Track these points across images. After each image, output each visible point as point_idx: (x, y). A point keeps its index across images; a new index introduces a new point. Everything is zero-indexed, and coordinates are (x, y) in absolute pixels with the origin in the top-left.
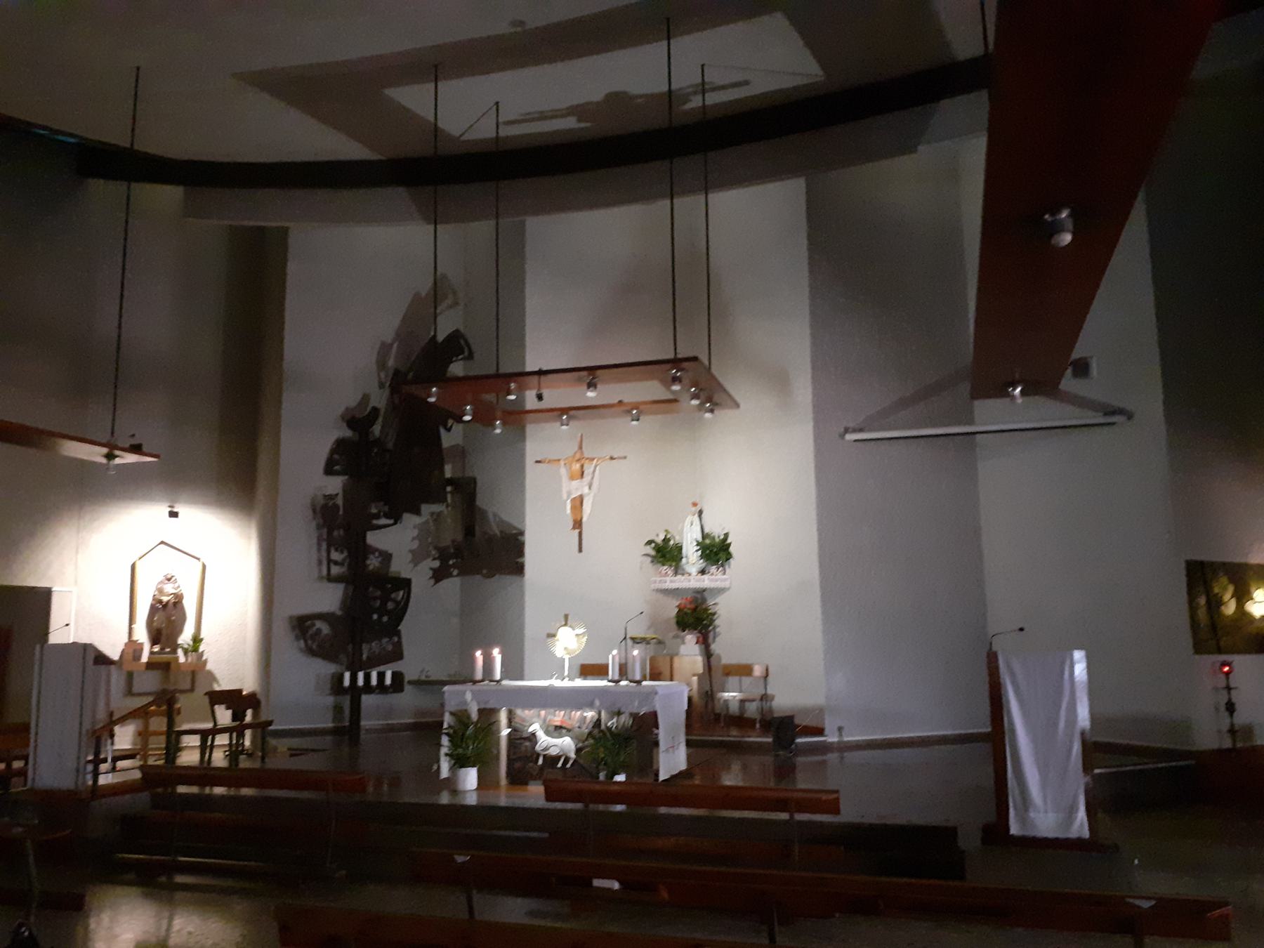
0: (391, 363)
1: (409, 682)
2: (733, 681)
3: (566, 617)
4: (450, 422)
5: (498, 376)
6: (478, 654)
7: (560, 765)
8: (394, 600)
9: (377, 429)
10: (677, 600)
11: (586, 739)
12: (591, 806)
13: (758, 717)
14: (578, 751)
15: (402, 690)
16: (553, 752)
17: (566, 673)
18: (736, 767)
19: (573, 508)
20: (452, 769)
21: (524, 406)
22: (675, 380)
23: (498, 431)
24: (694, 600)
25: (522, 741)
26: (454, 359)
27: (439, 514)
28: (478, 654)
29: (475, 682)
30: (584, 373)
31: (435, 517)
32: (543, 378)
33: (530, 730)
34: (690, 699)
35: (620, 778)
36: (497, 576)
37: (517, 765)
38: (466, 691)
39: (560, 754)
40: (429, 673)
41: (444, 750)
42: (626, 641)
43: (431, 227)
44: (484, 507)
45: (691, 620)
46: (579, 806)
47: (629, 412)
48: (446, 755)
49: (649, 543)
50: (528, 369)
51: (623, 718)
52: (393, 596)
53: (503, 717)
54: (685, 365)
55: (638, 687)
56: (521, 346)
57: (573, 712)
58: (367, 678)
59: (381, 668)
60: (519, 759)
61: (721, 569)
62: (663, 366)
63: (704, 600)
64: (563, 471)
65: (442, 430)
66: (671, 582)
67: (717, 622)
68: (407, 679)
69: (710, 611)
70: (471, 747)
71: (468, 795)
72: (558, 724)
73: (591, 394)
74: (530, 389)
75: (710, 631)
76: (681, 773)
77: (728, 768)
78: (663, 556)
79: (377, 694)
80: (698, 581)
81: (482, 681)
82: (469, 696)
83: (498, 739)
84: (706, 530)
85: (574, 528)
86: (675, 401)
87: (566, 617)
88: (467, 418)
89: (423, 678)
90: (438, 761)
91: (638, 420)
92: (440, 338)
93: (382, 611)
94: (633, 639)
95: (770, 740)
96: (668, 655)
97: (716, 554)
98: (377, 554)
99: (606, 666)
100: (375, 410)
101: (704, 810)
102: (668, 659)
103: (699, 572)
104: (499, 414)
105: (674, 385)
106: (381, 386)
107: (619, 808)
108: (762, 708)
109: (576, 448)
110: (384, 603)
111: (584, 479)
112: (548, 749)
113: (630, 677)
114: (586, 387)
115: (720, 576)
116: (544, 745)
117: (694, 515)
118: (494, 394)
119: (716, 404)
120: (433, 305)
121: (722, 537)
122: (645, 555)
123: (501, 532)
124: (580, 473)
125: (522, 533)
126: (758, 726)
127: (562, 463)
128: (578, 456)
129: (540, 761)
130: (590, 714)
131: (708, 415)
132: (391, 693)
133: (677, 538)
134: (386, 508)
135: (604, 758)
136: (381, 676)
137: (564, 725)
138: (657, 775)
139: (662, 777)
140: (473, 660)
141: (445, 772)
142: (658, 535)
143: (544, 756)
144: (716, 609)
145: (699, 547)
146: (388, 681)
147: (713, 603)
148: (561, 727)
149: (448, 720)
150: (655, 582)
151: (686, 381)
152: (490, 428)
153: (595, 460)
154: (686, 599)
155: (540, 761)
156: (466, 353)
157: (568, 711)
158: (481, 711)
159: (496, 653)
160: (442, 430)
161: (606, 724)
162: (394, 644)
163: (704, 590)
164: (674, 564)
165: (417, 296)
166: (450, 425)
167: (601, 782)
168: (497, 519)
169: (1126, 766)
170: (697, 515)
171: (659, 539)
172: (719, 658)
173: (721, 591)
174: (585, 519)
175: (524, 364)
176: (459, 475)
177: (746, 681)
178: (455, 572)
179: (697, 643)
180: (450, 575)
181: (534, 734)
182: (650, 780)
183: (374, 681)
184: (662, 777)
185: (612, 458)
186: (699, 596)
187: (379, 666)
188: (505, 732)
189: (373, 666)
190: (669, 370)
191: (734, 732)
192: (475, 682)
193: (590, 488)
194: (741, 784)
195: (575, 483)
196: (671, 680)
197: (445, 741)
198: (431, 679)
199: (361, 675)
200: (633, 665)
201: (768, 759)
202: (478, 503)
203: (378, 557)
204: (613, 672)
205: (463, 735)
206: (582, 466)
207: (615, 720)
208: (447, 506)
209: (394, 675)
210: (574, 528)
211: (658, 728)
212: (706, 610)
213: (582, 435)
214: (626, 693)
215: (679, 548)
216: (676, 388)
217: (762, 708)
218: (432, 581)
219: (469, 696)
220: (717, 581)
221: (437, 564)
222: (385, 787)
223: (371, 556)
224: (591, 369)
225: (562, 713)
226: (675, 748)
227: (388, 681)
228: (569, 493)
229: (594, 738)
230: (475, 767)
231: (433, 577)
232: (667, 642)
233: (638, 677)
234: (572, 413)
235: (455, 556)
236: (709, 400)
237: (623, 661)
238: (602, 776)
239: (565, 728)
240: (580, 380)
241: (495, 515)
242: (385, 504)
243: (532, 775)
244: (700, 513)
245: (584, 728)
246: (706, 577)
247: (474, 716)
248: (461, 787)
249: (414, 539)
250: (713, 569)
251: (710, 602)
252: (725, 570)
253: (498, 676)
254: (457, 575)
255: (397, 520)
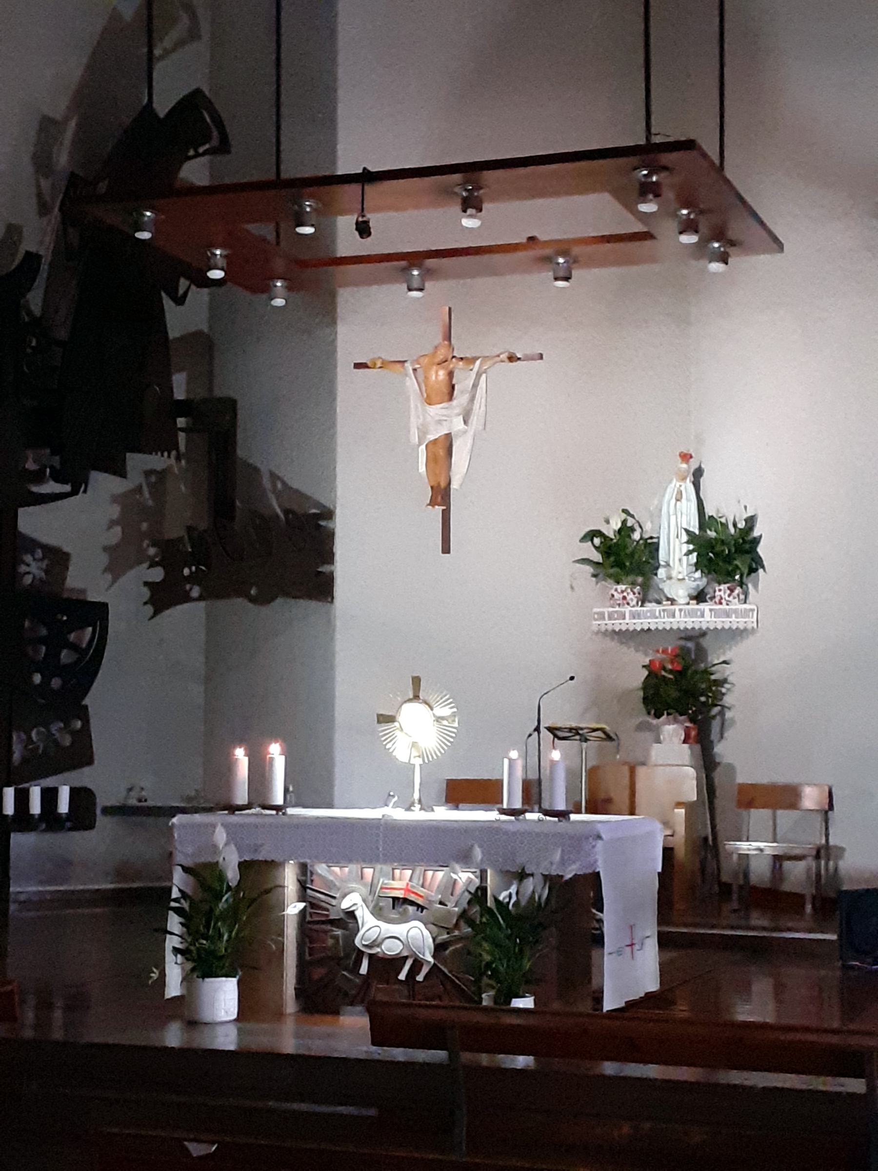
0: (63, 159)
1: (107, 811)
2: (759, 816)
3: (416, 682)
4: (183, 283)
5: (279, 184)
6: (240, 753)
7: (402, 976)
8: (74, 647)
9: (35, 300)
10: (646, 655)
11: (457, 926)
12: (466, 1057)
13: (809, 891)
14: (439, 948)
15: (91, 826)
16: (391, 949)
17: (416, 796)
18: (762, 986)
19: (432, 460)
20: (186, 979)
21: (334, 251)
22: (647, 190)
23: (279, 302)
24: (682, 654)
25: (329, 927)
26: (191, 153)
27: (162, 475)
28: (240, 753)
29: (233, 809)
30: (457, 177)
31: (153, 479)
32: (371, 190)
33: (345, 904)
34: (668, 852)
35: (525, 1003)
36: (279, 601)
37: (319, 973)
38: (214, 826)
39: (402, 955)
40: (144, 793)
41: (172, 942)
42: (539, 733)
43: (832, 842)
44: (255, 461)
45: (674, 694)
46: (439, 1055)
47: (548, 260)
48: (176, 951)
49: (591, 535)
50: (342, 170)
51: (529, 885)
52: (72, 637)
53: (289, 877)
54: (668, 158)
55: (564, 824)
56: (330, 123)
57: (430, 874)
58: (22, 799)
59: (49, 782)
60: (320, 962)
61: (738, 590)
62: (622, 161)
63: (701, 652)
64: (411, 383)
65: (168, 303)
66: (634, 616)
67: (728, 700)
68: (102, 801)
69: (713, 677)
70: (226, 937)
71: (220, 1031)
72: (400, 894)
73: (468, 223)
74: (343, 213)
75: (714, 717)
76: (649, 996)
77: (744, 989)
78: (619, 564)
79: (45, 831)
80: (691, 614)
81: (248, 806)
82: (220, 836)
83: (282, 920)
84: (710, 511)
85: (433, 503)
86: (647, 236)
87: (416, 682)
88: (216, 274)
89: (133, 802)
90: (161, 965)
91: (567, 279)
92: (162, 107)
93: (50, 667)
94: (550, 729)
95: (834, 937)
96: (625, 763)
97: (729, 559)
98: (39, 553)
99: (499, 783)
100: (32, 259)
101: (693, 1070)
102: (626, 770)
103: (692, 598)
104: (279, 264)
105: (644, 202)
106: (44, 209)
107: (522, 1061)
108: (818, 874)
109: (439, 339)
110: (53, 655)
111: (454, 403)
112: (379, 946)
113: (546, 805)
114: (458, 208)
115: (736, 605)
116: (373, 935)
117: (684, 479)
118: (271, 226)
119: (732, 243)
120: (144, 39)
121: (741, 525)
122: (578, 561)
123: (287, 512)
124: (445, 390)
125: (329, 514)
126: (809, 908)
127: (409, 367)
128: (441, 355)
129: (364, 969)
130: (464, 877)
131: (716, 267)
132: (70, 829)
133: (648, 526)
134: (56, 461)
135: (491, 963)
136: (50, 797)
137: (412, 897)
138: (598, 998)
139: (609, 1004)
140: (230, 766)
141: (174, 988)
142: (608, 522)
143: (371, 956)
144: (727, 673)
145: (691, 547)
146: (63, 807)
147: (721, 660)
148: (405, 901)
149: (179, 880)
150: (601, 616)
151: (669, 194)
152: (264, 296)
153: (478, 362)
154: (665, 651)
155: (364, 969)
156: (215, 142)
157: (419, 870)
158: (244, 866)
159: (275, 750)
160: (168, 303)
161: (496, 900)
162: (74, 733)
163: (703, 634)
164: (640, 579)
165: (115, 16)
166: (181, 292)
167: (486, 1009)
168: (279, 486)
169: (797, 931)
170: (690, 479)
171: (611, 529)
172: (731, 768)
173: (736, 635)
174: (454, 486)
175: (334, 162)
176: (201, 393)
177: (785, 817)
178: (195, 592)
179: (685, 742)
180: (186, 598)
181: (351, 914)
182: (585, 1007)
183: (36, 808)
184: (609, 1004)
185: (512, 358)
186: (690, 645)
187: (47, 776)
188: (294, 909)
189: (34, 777)
190: (635, 169)
191: (758, 919)
192: (233, 809)
193: (466, 422)
194: (770, 1019)
195: (435, 411)
196: (632, 813)
197: (174, 923)
198: (150, 803)
199: (35, 794)
200: (552, 779)
201: (831, 973)
202: (240, 453)
203: (42, 560)
204: (512, 797)
205: (211, 910)
206: (451, 374)
207: (513, 889)
208: (178, 459)
209: (75, 793)
210: (433, 503)
211: (601, 910)
212: (707, 672)
213: (450, 309)
214: (533, 835)
215: (652, 547)
216: (648, 207)
217: (818, 874)
218: (150, 609)
219: (220, 836)
220: (727, 614)
221: (157, 575)
222: (58, 1014)
223: (28, 558)
224: (471, 169)
225: (408, 873)
226: (636, 947)
227: (63, 807)
228: (423, 432)
229: (471, 922)
230: (235, 977)
231: (151, 601)
232: (623, 737)
233: (561, 806)
234: (430, 262)
235: (194, 559)
236: (719, 234)
237: (533, 776)
238: (486, 999)
239: (412, 903)
240: (447, 192)
241: (274, 477)
242: (53, 453)
243: (346, 994)
244: (698, 473)
245: (450, 905)
246: (705, 607)
247: (232, 875)
248: (207, 1015)
249: (112, 523)
250: (722, 591)
251: (714, 658)
252: (746, 594)
253: (279, 800)
254: (200, 598)
255: (78, 484)
